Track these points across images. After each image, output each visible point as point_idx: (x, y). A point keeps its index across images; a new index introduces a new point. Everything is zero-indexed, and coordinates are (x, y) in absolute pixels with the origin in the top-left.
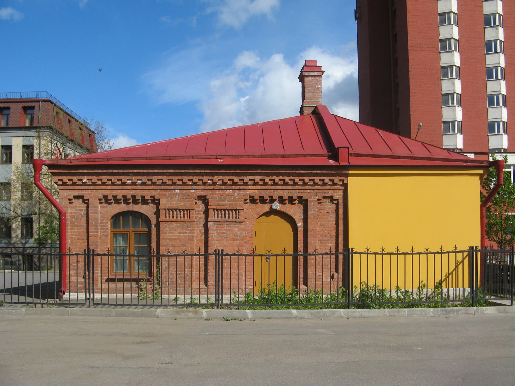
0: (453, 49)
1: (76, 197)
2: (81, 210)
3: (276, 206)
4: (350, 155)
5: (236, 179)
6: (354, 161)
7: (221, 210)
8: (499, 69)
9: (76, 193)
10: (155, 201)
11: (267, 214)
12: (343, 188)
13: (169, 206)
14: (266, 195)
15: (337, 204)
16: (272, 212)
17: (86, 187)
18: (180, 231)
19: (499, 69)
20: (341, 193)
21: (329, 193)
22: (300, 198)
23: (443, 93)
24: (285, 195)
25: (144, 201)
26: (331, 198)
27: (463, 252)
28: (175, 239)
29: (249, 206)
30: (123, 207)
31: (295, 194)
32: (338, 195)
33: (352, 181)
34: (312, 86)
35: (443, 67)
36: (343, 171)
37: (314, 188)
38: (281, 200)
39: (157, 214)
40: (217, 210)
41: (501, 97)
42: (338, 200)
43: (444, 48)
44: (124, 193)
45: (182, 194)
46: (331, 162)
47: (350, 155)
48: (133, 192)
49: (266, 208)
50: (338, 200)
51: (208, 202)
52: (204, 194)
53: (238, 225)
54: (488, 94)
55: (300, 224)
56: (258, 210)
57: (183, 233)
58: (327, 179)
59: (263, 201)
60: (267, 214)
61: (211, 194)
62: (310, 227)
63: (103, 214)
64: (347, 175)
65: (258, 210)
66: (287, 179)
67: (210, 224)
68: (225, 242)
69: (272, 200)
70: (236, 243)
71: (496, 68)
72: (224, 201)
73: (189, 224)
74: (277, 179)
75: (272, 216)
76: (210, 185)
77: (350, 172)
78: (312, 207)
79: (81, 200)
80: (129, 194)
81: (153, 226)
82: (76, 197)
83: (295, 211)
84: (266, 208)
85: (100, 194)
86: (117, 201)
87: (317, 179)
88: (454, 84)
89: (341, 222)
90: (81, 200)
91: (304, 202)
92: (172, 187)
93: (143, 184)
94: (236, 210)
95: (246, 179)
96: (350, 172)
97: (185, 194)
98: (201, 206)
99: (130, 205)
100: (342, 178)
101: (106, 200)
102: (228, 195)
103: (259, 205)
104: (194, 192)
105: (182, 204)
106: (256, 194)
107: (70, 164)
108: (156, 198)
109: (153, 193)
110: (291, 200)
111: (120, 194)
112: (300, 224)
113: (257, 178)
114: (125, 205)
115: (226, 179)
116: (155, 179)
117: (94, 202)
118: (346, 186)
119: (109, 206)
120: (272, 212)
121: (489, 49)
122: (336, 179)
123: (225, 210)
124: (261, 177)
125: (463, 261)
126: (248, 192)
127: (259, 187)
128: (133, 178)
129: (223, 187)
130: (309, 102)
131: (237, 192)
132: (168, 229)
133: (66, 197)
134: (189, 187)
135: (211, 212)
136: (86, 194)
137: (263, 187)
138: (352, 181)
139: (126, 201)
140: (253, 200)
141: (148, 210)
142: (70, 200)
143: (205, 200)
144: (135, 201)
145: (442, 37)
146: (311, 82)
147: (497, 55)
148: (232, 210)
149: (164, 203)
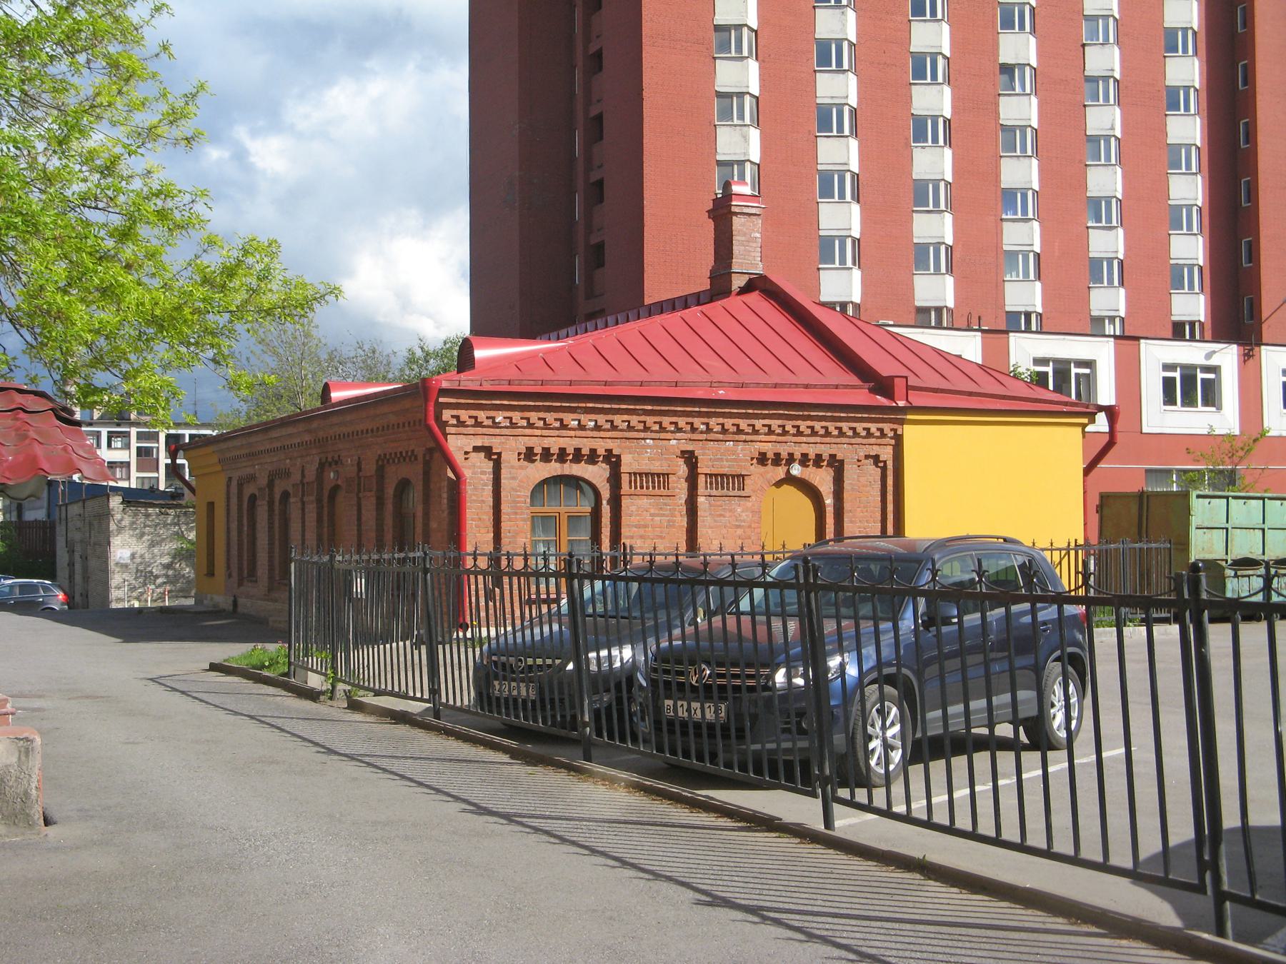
0: (745, 53)
1: (476, 449)
2: (483, 473)
3: (796, 470)
4: (908, 388)
5: (743, 424)
6: (917, 399)
7: (716, 475)
8: (846, 109)
9: (479, 442)
10: (613, 461)
11: (778, 484)
12: (893, 442)
13: (636, 468)
14: (784, 451)
15: (884, 469)
16: (789, 480)
17: (498, 431)
18: (652, 511)
19: (846, 109)
20: (890, 450)
21: (874, 451)
22: (833, 456)
23: (719, 158)
24: (812, 451)
25: (592, 458)
26: (876, 459)
27: (1060, 550)
28: (646, 526)
29: (756, 469)
30: (554, 468)
31: (826, 451)
32: (887, 454)
33: (913, 435)
34: (745, 235)
35: (720, 95)
36: (897, 415)
37: (853, 441)
38: (804, 460)
39: (615, 479)
40: (711, 475)
41: (848, 177)
42: (885, 462)
43: (725, 47)
44: (563, 442)
45: (657, 447)
46: (881, 400)
47: (908, 388)
48: (577, 443)
49: (780, 472)
50: (885, 462)
51: (697, 462)
52: (690, 448)
53: (743, 502)
54: (820, 167)
55: (829, 501)
56: (769, 476)
57: (658, 515)
58: (873, 427)
59: (777, 460)
60: (778, 484)
61: (702, 448)
62: (847, 506)
63: (522, 478)
64: (902, 422)
65: (769, 476)
66: (818, 426)
67: (701, 500)
68: (724, 531)
69: (791, 459)
70: (739, 532)
71: (840, 107)
72: (721, 460)
73: (667, 500)
74: (803, 425)
75: (785, 487)
76: (702, 432)
77: (909, 417)
78: (850, 473)
79: (482, 455)
80: (570, 444)
81: (604, 502)
82: (476, 449)
83: (823, 479)
84: (780, 472)
85: (521, 444)
86: (546, 455)
87: (860, 427)
88: (746, 138)
89: (890, 498)
90: (482, 455)
91: (837, 466)
92: (642, 435)
93: (597, 428)
94: (738, 476)
95: (758, 424)
96: (909, 417)
97: (661, 448)
98: (683, 470)
99: (567, 465)
100: (895, 426)
101: (529, 455)
102: (728, 449)
103: (770, 467)
104: (676, 443)
105: (658, 464)
106: (769, 449)
107: (479, 388)
108: (615, 452)
109: (610, 444)
110: (818, 461)
111: (554, 444)
112: (829, 501)
113: (775, 423)
114: (558, 465)
115: (729, 423)
116: (618, 419)
117: (509, 459)
118: (899, 439)
119: (531, 465)
120: (789, 480)
121: (824, 60)
122: (887, 427)
123: (722, 476)
124: (780, 422)
125: (1060, 563)
126: (757, 445)
127: (773, 438)
128: (582, 417)
129: (720, 437)
130: (741, 265)
131: (741, 445)
132: (633, 508)
133: (461, 448)
134: (668, 436)
135: (701, 479)
136: (496, 444)
137: (781, 438)
138: (913, 435)
139: (562, 456)
140: (762, 459)
141: (597, 474)
142: (466, 453)
143: (690, 459)
144: (578, 456)
145: (720, 19)
146: (743, 225)
147: (841, 76)
148: (733, 476)
149: (629, 463)
